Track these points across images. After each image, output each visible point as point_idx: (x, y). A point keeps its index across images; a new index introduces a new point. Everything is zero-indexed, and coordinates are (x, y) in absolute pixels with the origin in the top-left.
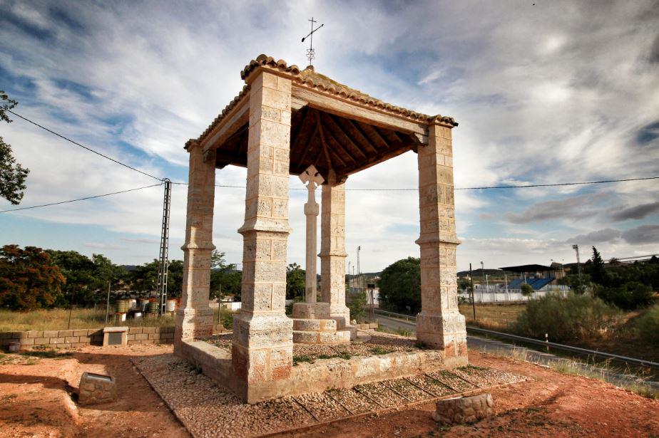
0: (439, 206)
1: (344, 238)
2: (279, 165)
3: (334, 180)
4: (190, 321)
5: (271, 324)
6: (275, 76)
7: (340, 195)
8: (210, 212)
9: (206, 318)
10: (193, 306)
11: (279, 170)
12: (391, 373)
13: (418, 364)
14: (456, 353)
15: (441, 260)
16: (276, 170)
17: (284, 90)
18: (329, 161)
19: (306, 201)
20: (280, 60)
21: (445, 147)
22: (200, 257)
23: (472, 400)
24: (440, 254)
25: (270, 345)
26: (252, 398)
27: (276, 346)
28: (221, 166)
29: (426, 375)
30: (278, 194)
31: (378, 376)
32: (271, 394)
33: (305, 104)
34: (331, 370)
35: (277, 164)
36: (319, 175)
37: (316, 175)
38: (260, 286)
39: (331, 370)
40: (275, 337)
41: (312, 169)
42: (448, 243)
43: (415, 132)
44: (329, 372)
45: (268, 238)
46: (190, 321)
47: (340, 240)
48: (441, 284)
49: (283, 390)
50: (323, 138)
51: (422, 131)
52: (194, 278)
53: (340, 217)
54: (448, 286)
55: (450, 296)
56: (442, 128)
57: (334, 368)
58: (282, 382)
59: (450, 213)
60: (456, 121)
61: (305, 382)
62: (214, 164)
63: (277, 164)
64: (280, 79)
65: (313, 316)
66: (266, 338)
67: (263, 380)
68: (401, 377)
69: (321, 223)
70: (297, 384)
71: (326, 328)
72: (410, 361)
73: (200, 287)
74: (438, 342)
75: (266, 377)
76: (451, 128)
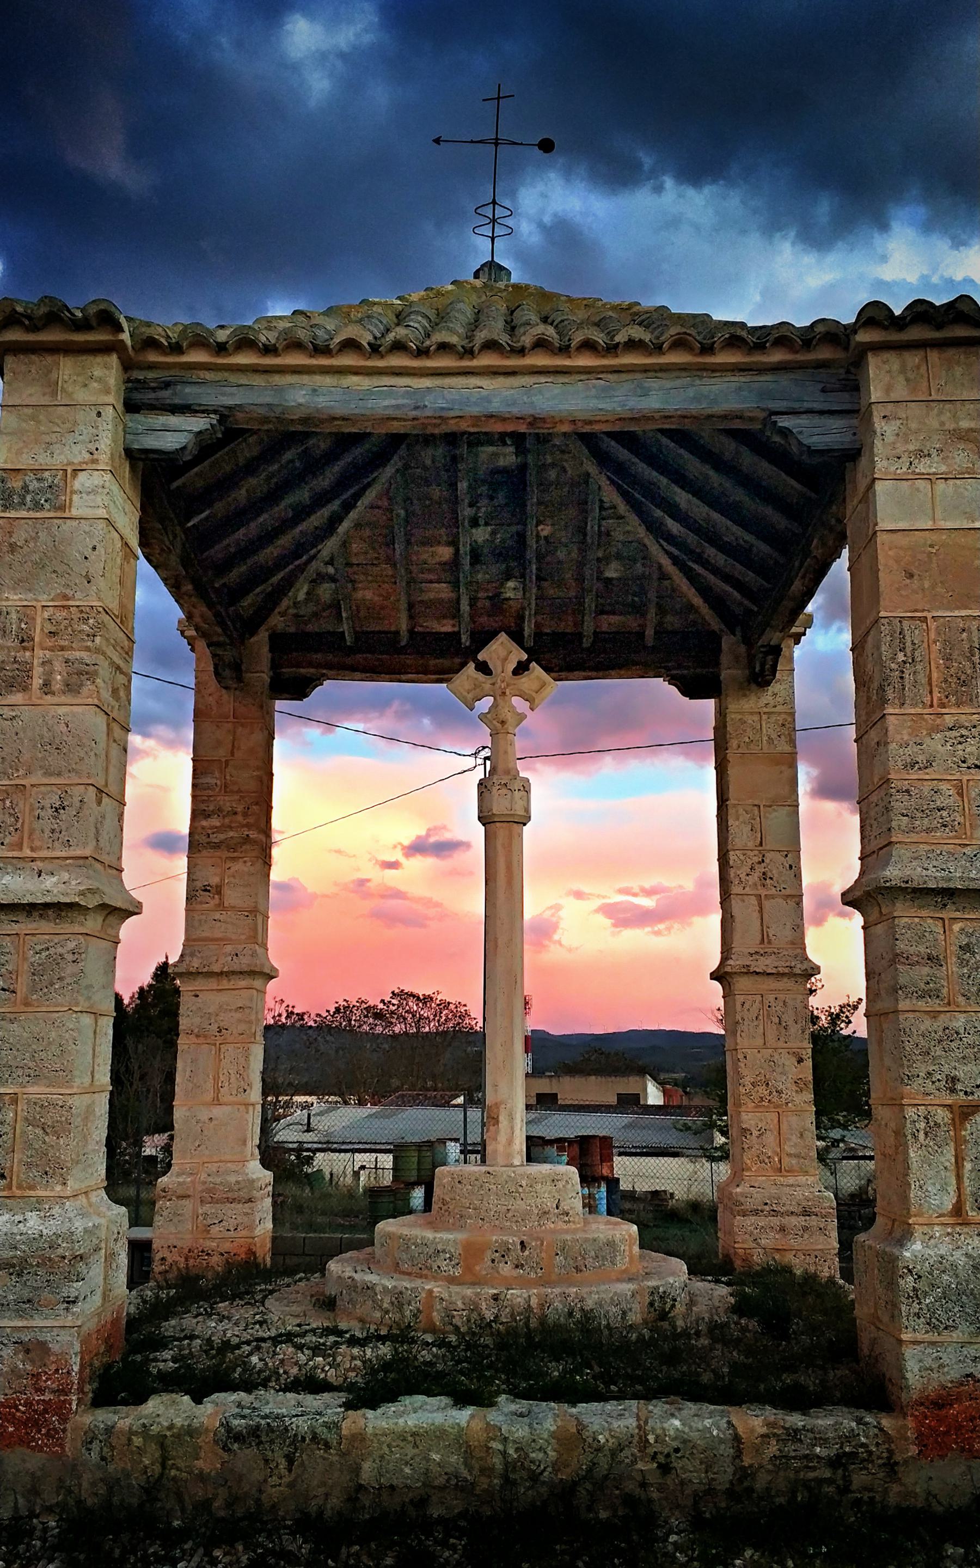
2: (58, 666)
6: (49, 359)
7: (769, 729)
16: (47, 687)
17: (81, 396)
18: (697, 601)
33: (198, 423)
37: (521, 668)
41: (502, 652)
50: (633, 519)
56: (913, 358)
64: (66, 367)
69: (233, 817)
71: (483, 1268)
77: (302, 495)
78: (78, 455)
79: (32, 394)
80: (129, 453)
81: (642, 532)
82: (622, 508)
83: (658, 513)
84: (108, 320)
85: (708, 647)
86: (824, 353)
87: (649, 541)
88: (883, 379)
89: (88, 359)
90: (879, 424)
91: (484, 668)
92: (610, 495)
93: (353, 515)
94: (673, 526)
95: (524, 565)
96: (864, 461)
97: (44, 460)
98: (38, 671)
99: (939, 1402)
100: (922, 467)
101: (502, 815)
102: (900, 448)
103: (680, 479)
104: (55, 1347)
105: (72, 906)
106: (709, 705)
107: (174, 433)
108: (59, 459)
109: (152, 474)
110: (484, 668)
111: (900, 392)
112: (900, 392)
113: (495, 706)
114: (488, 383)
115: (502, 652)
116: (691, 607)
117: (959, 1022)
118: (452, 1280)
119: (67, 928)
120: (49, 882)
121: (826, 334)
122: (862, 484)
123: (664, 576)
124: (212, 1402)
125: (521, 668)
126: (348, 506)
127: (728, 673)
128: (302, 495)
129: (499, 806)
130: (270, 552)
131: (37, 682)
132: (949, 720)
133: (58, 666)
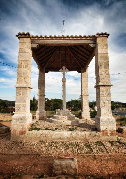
0: (99, 71)
1: (88, 89)
2: (24, 65)
3: (83, 71)
4: (38, 114)
5: (19, 117)
6: (23, 38)
7: (85, 75)
8: (44, 85)
9: (42, 114)
10: (39, 111)
11: (24, 67)
12: (70, 139)
13: (84, 137)
14: (109, 134)
15: (101, 93)
16: (23, 68)
17: (26, 42)
18: (80, 65)
19: (62, 78)
20: (23, 33)
21: (103, 46)
22: (41, 97)
23: (60, 163)
24: (100, 91)
25: (18, 123)
26: (12, 140)
27: (20, 124)
28: (47, 72)
29: (88, 142)
30: (23, 75)
31: (63, 139)
32: (18, 139)
33: (38, 44)
34: (41, 134)
35: (23, 65)
36: (67, 69)
37: (65, 69)
38: (17, 105)
39: (41, 134)
40: (20, 121)
41: (64, 68)
42: (105, 86)
43: (88, 43)
44: (41, 135)
45: (20, 89)
46: (38, 114)
47: (86, 90)
48: (101, 104)
49: (23, 139)
50: (75, 58)
51: (92, 42)
52: (39, 103)
53: (86, 83)
54: (105, 104)
55: (106, 109)
56: (101, 38)
57: (42, 134)
58: (22, 136)
59: (107, 73)
60: (108, 33)
61: (31, 137)
62: (44, 71)
63: (23, 65)
64: (25, 39)
65: (61, 115)
66: (17, 121)
67: (16, 134)
68: (75, 141)
69: (42, 83)
70: (28, 137)
71: (63, 119)
72: (80, 135)
73: (41, 105)
74: (99, 128)
75: (17, 134)
76: (107, 37)
77: (47, 55)
78: (26, 47)
79: (22, 41)
80: (31, 47)
81: (75, 59)
82: (74, 57)
83: (77, 57)
84: (28, 34)
85: (81, 68)
86: (93, 38)
87: (76, 60)
88: (99, 40)
89: (27, 38)
90: (98, 44)
91: (62, 69)
92: (73, 56)
93: (51, 57)
94: (78, 58)
95: (65, 61)
96: (96, 48)
97: (23, 47)
98: (23, 66)
99: (103, 131)
100: (102, 48)
101: (64, 81)
102: (100, 46)
103: (78, 53)
104: (25, 126)
105: (26, 87)
106: (80, 74)
107: (35, 45)
108: (25, 47)
109: (33, 49)
110: (62, 69)
111: (100, 41)
112: (100, 41)
113: (45, 175)
114: (63, 41)
115: (64, 68)
116: (79, 65)
117: (105, 97)
118: (60, 120)
119: (25, 89)
120: (24, 85)
121: (94, 36)
122: (96, 50)
123: (77, 63)
124: (110, 83)
125: (65, 69)
126: (51, 56)
127: (82, 71)
128: (47, 55)
129: (64, 80)
130: (44, 60)
131: (23, 67)
132: (104, 71)
133: (24, 65)
